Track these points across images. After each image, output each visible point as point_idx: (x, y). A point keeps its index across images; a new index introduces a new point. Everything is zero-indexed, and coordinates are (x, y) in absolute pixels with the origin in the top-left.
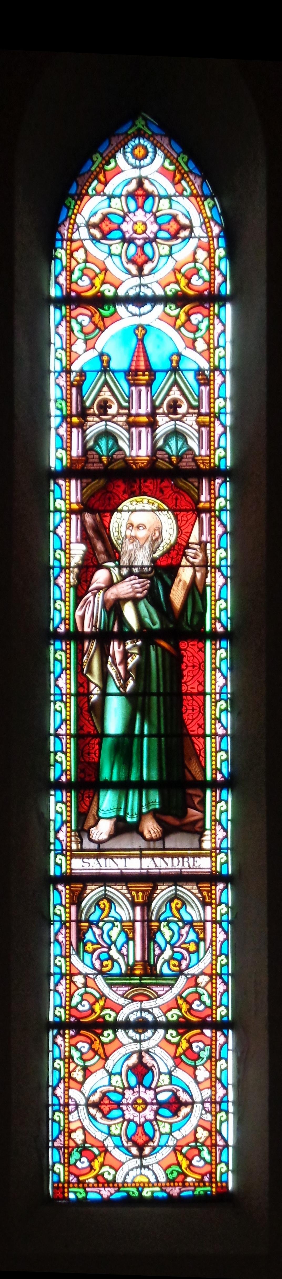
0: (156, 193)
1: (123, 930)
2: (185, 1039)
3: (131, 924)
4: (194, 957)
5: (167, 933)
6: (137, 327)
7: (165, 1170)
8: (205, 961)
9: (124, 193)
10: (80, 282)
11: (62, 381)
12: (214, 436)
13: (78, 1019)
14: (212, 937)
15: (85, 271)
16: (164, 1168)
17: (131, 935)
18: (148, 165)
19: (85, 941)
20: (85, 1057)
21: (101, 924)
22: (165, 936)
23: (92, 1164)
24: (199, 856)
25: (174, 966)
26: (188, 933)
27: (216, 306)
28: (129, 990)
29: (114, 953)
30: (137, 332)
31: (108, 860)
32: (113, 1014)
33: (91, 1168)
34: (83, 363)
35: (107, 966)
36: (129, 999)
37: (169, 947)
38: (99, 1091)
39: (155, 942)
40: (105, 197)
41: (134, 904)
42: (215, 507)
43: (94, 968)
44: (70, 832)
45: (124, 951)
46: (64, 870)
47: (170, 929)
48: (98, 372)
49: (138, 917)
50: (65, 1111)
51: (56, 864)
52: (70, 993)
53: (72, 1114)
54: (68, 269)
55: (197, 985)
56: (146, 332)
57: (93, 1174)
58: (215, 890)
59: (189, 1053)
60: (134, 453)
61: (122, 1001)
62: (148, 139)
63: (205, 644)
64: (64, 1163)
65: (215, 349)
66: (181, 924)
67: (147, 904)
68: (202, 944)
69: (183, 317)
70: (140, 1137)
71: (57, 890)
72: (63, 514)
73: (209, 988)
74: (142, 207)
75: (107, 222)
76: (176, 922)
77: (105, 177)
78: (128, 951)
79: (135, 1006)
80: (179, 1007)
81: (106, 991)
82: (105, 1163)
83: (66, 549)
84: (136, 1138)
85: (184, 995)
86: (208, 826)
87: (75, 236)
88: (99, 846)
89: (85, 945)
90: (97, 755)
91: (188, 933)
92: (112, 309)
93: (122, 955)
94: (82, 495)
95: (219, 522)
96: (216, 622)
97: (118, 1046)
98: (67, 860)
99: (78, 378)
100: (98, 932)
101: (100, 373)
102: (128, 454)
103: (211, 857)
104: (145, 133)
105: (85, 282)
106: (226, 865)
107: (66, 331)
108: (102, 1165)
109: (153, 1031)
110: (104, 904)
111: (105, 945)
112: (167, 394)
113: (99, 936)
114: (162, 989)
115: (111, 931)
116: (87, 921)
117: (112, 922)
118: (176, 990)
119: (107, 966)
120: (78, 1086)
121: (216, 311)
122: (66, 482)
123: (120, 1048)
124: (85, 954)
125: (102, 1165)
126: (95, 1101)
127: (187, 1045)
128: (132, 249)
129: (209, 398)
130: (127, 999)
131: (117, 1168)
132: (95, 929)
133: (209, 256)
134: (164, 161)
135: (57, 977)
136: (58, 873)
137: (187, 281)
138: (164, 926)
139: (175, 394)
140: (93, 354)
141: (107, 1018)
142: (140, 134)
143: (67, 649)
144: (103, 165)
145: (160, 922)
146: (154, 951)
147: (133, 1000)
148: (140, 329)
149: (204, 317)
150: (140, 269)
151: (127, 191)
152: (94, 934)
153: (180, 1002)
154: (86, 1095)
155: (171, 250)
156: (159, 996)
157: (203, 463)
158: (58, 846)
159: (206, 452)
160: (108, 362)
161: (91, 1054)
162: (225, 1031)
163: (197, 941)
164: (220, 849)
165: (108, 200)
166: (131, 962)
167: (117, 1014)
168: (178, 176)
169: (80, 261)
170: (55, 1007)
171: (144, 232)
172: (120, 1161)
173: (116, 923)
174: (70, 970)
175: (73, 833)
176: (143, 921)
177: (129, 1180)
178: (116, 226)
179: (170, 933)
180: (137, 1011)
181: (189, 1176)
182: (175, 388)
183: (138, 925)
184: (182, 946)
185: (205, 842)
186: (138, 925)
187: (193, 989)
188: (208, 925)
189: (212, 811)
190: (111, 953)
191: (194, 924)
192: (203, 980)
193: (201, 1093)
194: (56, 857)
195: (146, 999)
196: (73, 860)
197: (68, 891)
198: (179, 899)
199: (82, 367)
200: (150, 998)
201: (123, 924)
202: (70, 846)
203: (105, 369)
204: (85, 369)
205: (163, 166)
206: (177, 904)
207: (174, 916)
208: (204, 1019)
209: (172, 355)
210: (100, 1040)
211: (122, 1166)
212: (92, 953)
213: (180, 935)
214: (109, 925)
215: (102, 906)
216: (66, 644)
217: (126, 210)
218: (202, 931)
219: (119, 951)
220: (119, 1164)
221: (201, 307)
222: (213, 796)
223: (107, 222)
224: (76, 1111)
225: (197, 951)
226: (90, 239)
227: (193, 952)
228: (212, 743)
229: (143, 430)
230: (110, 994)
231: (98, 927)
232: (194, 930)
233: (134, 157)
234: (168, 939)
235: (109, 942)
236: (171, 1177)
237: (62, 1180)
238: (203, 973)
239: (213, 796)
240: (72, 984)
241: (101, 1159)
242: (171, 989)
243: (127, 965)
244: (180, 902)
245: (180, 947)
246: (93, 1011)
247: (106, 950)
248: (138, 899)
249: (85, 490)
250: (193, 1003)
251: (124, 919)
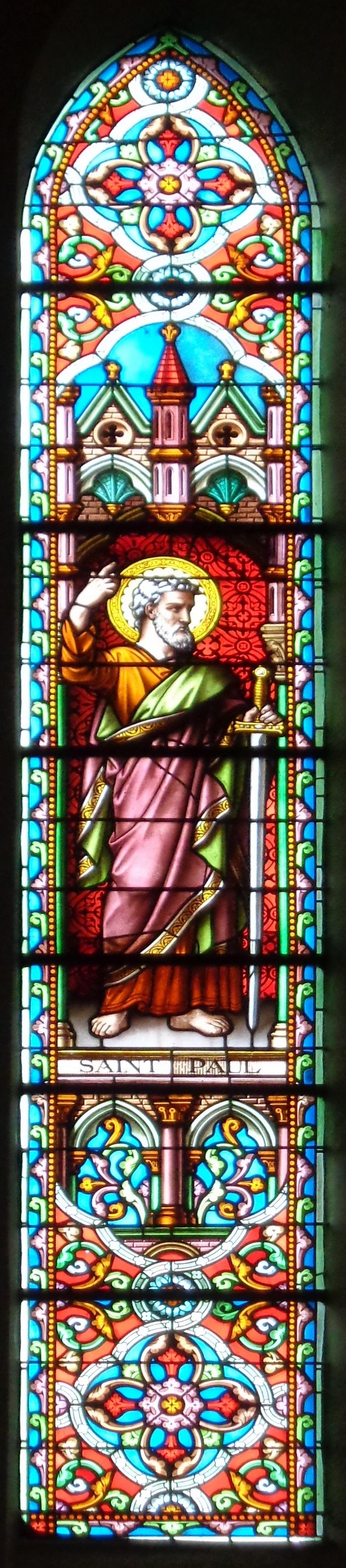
0: (194, 135)
1: (142, 1161)
2: (246, 1314)
3: (156, 1153)
4: (260, 1198)
5: (216, 1165)
6: (164, 326)
7: (210, 1498)
8: (276, 1206)
9: (142, 136)
10: (72, 262)
11: (42, 396)
12: (291, 479)
13: (69, 1286)
14: (289, 1173)
15: (80, 248)
16: (209, 1495)
17: (155, 1169)
18: (182, 98)
19: (79, 1176)
20: (81, 328)
21: (106, 1153)
22: (213, 1170)
23: (93, 1487)
25: (227, 1211)
26: (249, 1166)
27: (296, 296)
28: (153, 1245)
29: (127, 1193)
30: (164, 332)
32: (125, 1499)
33: (91, 1493)
34: (76, 373)
35: (115, 1211)
36: (153, 1258)
37: (218, 1184)
38: (104, 1385)
39: (195, 1177)
40: (113, 144)
41: (160, 1125)
42: (293, 575)
43: (94, 1213)
44: (56, 1023)
45: (144, 1190)
46: (45, 512)
47: (220, 1159)
48: (101, 386)
49: (168, 1142)
50: (50, 214)
51: (30, 1209)
52: (54, 1248)
53: (59, 1418)
54: (52, 241)
55: (263, 1239)
56: (179, 332)
57: (94, 1501)
58: (295, 1107)
59: (252, 1333)
60: (159, 499)
61: (140, 1261)
62: (183, 63)
63: (278, 972)
64: (48, 1486)
65: (294, 354)
66: (238, 1152)
67: (182, 1125)
68: (272, 1181)
69: (241, 313)
70: (170, 226)
71: (37, 539)
72: (46, 581)
73: (283, 1242)
74: (173, 157)
75: (117, 1399)
76: (229, 1150)
77: (112, 114)
78: (150, 1190)
79: (163, 1267)
80: (233, 1270)
81: (115, 1246)
82: (113, 1486)
83: (50, 491)
84: (165, 228)
85: (242, 1253)
86: (282, 1015)
87: (64, 199)
88: (102, 1042)
89: (80, 1181)
90: (99, 914)
91: (249, 1166)
92: (126, 301)
93: (141, 1196)
94: (77, 554)
95: (303, 805)
96: (283, 176)
97: (134, 1326)
98: (50, 1062)
99: (67, 394)
100: (101, 1163)
101: (104, 387)
102: (149, 500)
104: (180, 54)
105: (82, 261)
106: (313, 928)
107: (50, 328)
108: (109, 1489)
109: (191, 294)
110: (112, 1124)
111: (112, 1182)
112: (214, 418)
113: (103, 1169)
114: (206, 1243)
115: (123, 1163)
116: (84, 1148)
117: (125, 1150)
118: (228, 1246)
119: (115, 1211)
120: (71, 1378)
121: (296, 303)
122: (50, 536)
123: (138, 1327)
124: (80, 1193)
125: (109, 1489)
126: (99, 1399)
127: (249, 1323)
128: (157, 216)
129: (284, 422)
131: (133, 267)
132: (97, 1160)
133: (283, 226)
134: (208, 94)
135: (34, 1155)
137: (249, 1487)
138: (211, 1155)
139: (228, 417)
140: (91, 361)
141: (114, 1503)
143: (49, 768)
144: (109, 99)
145: (204, 1149)
146: (193, 1190)
147: (159, 1258)
148: (169, 328)
149: (277, 312)
150: (171, 243)
151: (147, 134)
152: (95, 1166)
153: (236, 1262)
154: (83, 1393)
155: (220, 218)
156: (202, 1254)
157: (273, 514)
158: (34, 1221)
159: (277, 441)
160: (118, 373)
161: (91, 1333)
162: (312, 1305)
163: (264, 1176)
164: (302, 1048)
165: (115, 149)
166: (155, 1206)
167: (132, 1498)
168: (231, 115)
169: (72, 233)
170: (30, 913)
171: (177, 191)
172: (137, 1484)
173: (130, 1152)
174: (54, 1216)
175: (60, 1025)
176: (175, 1148)
177: (153, 1509)
178: (131, 184)
179: (221, 1165)
180: (164, 1493)
181: (249, 1506)
182: (227, 410)
183: (167, 1155)
184: (240, 1183)
185: (275, 1039)
186: (167, 1155)
187: (256, 238)
188: (284, 1153)
189: (289, 997)
190: (123, 1193)
191: (261, 1153)
192: (273, 1232)
193: (271, 1391)
194: (32, 216)
195: (180, 1258)
196: (60, 1062)
197: (52, 1108)
198: (234, 1118)
199: (74, 380)
200: (187, 1257)
201: (144, 1153)
202: (56, 1043)
203: (114, 383)
204: (79, 381)
205: (206, 99)
206: (232, 1125)
207: (226, 1141)
208: (273, 279)
209: (222, 364)
210: (106, 1315)
211: (140, 1491)
212: (92, 1193)
213: (237, 1167)
214: (119, 1155)
215: (108, 1126)
216: (49, 762)
217: (146, 160)
218: (273, 1163)
219: (136, 1191)
221: (271, 299)
222: (291, 977)
223: (117, 1399)
224: (67, 1414)
225: (265, 1190)
226: (89, 205)
227: (259, 1192)
228: (288, 831)
229: (175, 467)
230: (121, 1251)
231: (101, 1157)
232: (260, 1162)
233: (158, 88)
234: (217, 1173)
235: (119, 1177)
236: (221, 1507)
237: (44, 1508)
238: (273, 1222)
239: (291, 977)
240: (58, 1344)
241: (106, 1481)
242: (220, 1244)
243: (149, 1209)
244: (236, 1124)
245: (235, 1184)
246: (92, 1274)
247: (115, 1188)
248: (168, 1118)
249: (82, 547)
250: (257, 1482)
251: (145, 1145)
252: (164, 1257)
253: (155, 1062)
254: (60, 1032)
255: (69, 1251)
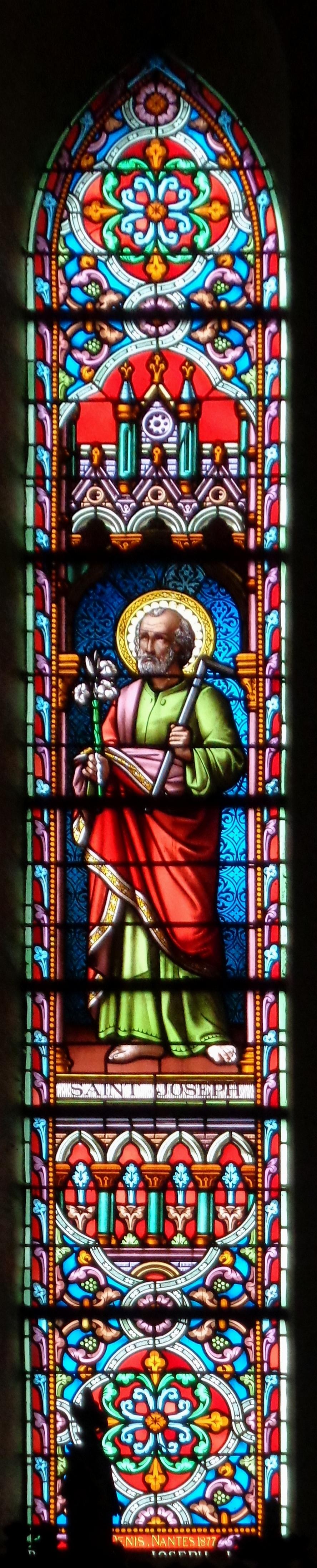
24: (238, 1082)
31: (108, 1086)
79: (146, 1288)
103: (255, 1083)
114: (126, 1264)
130: (136, 1278)
136: (37, 1102)
142: (157, 78)
147: (145, 1279)
148: (157, 358)
156: (182, 1273)
195: (161, 1278)
200: (167, 1278)
220: (128, 1501)
252: (150, 1277)
253: (136, 1086)
254: (58, 1062)
255: (86, 1271)
